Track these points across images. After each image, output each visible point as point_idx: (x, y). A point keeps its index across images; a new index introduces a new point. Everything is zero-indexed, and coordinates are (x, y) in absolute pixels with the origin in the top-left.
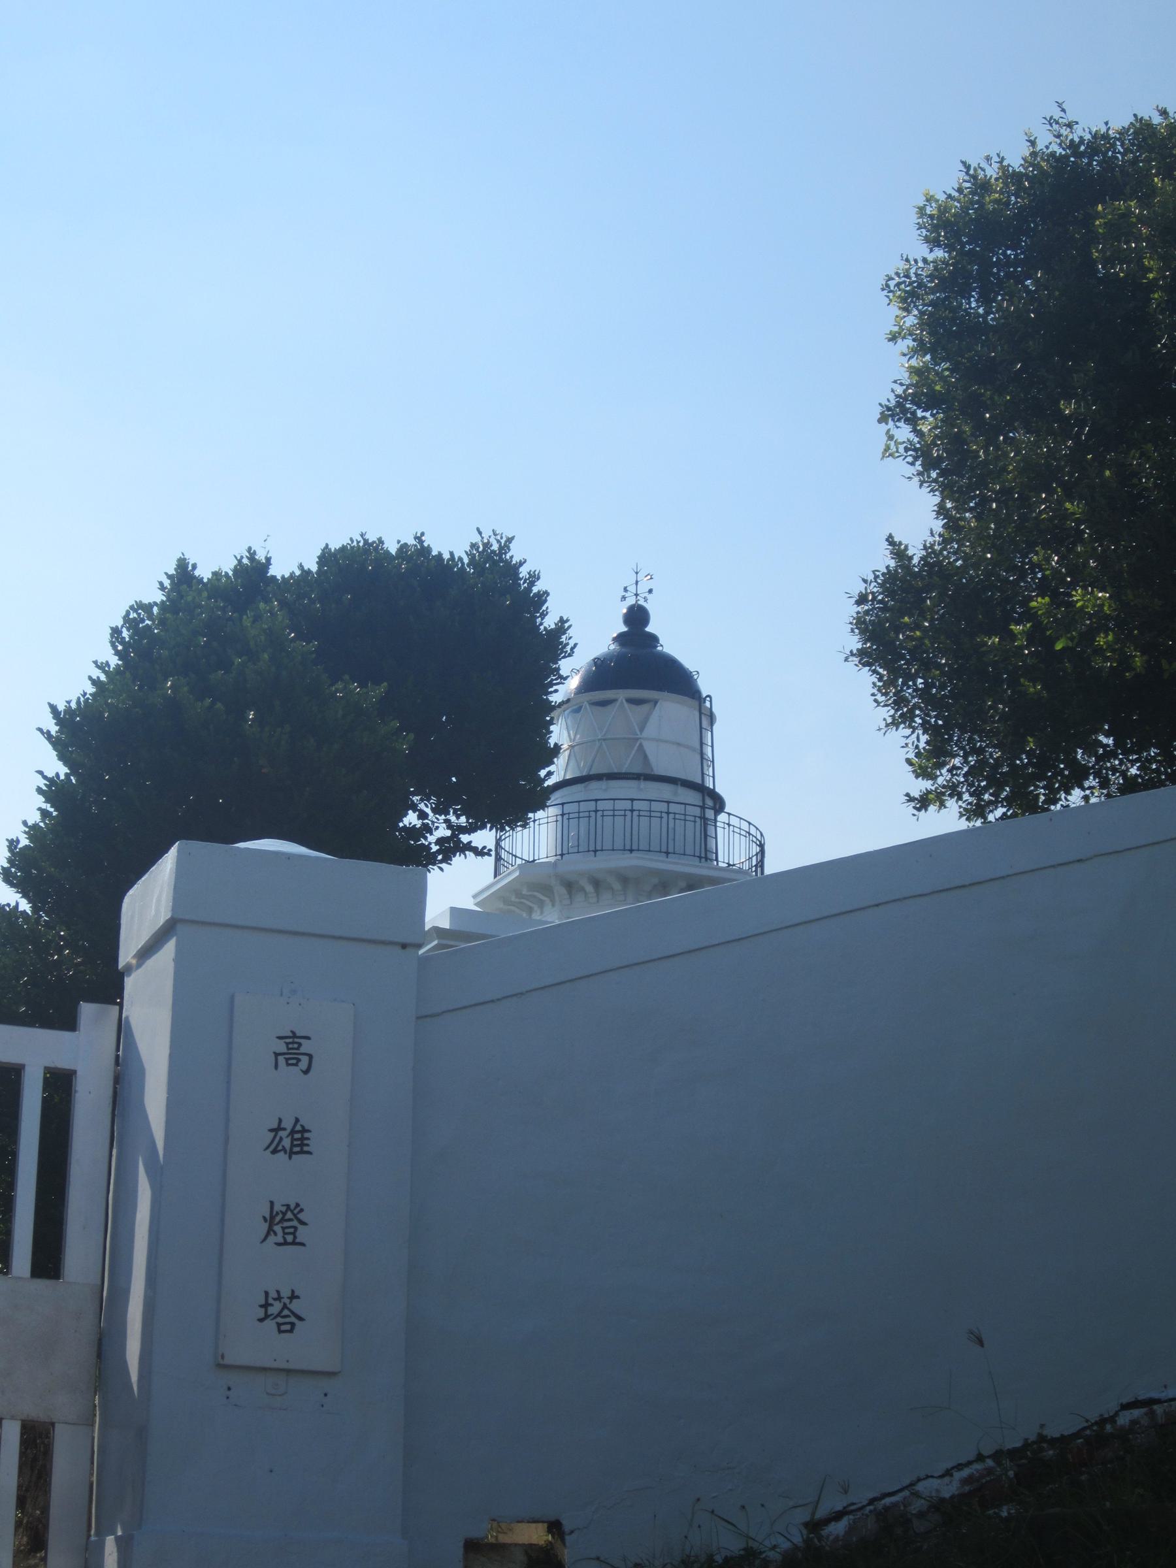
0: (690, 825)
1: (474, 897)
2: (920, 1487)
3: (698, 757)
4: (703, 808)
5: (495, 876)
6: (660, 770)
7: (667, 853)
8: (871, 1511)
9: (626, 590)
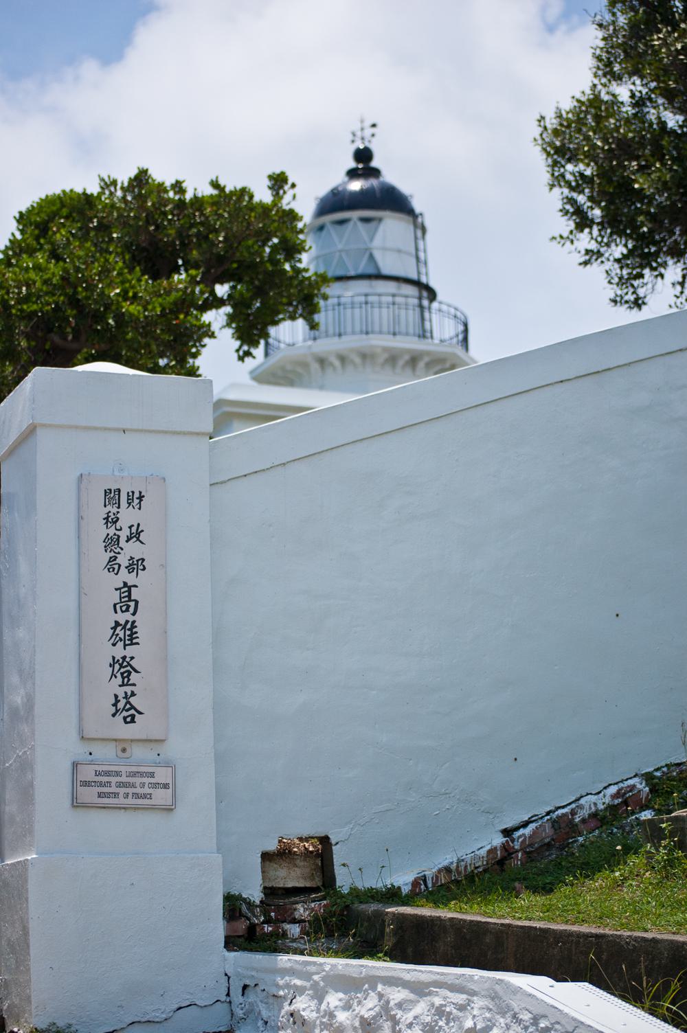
0: (411, 312)
2: (582, 801)
3: (414, 261)
4: (420, 298)
6: (386, 271)
7: (394, 334)
8: (548, 820)
9: (354, 135)
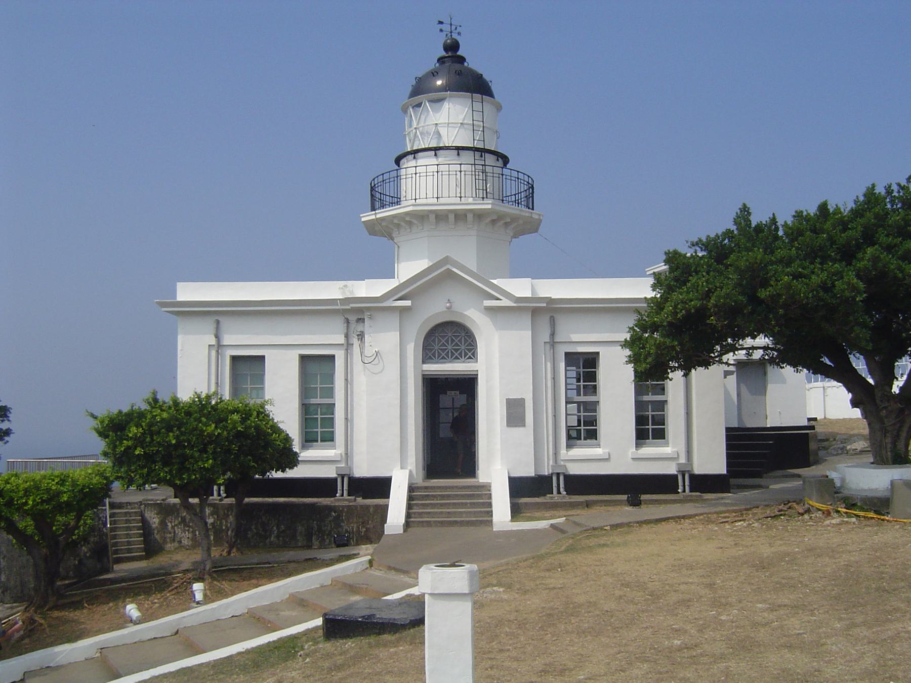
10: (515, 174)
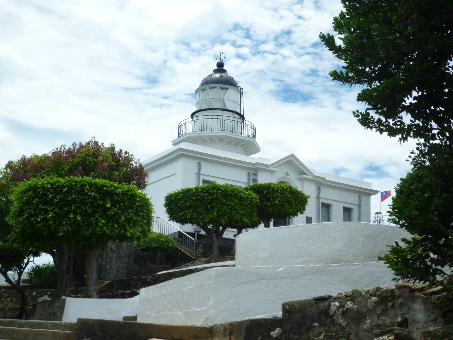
1: (172, 142)
5: (178, 137)
6: (228, 108)
10: (247, 123)
